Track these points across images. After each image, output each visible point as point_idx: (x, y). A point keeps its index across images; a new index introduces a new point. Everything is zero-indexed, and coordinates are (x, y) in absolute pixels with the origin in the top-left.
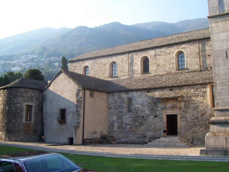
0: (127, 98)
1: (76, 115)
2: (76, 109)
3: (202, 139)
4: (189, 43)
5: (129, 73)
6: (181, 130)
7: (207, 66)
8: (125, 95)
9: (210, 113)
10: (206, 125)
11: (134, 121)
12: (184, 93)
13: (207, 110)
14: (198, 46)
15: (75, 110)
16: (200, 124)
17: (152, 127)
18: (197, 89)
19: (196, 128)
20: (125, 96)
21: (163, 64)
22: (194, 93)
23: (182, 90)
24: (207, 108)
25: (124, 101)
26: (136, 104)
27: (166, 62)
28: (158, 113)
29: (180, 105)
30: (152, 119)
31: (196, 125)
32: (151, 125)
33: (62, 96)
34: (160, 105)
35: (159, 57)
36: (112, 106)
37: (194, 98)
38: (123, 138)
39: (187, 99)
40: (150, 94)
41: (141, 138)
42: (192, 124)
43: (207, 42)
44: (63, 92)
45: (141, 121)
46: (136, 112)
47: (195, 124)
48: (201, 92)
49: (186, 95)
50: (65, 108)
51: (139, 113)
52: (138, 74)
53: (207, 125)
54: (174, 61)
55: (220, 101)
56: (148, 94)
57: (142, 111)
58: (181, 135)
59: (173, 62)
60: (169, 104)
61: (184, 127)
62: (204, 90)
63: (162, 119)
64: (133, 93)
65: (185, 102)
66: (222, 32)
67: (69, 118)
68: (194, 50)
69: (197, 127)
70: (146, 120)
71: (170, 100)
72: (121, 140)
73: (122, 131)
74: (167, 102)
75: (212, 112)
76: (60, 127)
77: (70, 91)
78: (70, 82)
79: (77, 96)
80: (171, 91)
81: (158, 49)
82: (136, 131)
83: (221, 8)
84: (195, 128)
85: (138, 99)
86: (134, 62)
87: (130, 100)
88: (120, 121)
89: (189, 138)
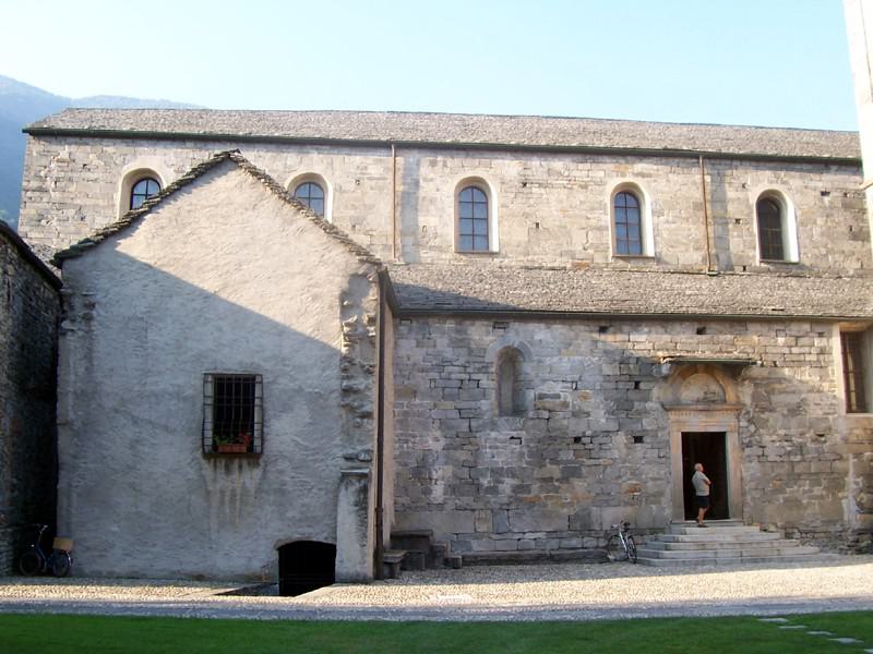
0: (499, 348)
1: (336, 412)
2: (343, 378)
5: (398, 241)
7: (729, 258)
8: (488, 333)
9: (845, 432)
11: (539, 458)
12: (750, 346)
13: (834, 419)
15: (335, 384)
16: (813, 470)
18: (797, 337)
19: (800, 486)
20: (491, 338)
21: (557, 223)
22: (786, 350)
23: (746, 334)
24: (834, 413)
25: (486, 360)
26: (544, 381)
27: (570, 217)
28: (647, 423)
29: (738, 397)
30: (625, 451)
31: (799, 475)
32: (620, 477)
33: (232, 299)
34: (658, 392)
35: (543, 191)
36: (421, 381)
37: (787, 372)
38: (477, 535)
39: (765, 372)
40: (612, 339)
41: (572, 536)
42: (783, 470)
43: (729, 172)
44: (237, 276)
45: (571, 456)
46: (546, 415)
47: (797, 470)
48: (813, 350)
49: (761, 355)
50: (251, 371)
51: (564, 421)
52: (440, 249)
53: (836, 476)
54: (603, 217)
56: (603, 337)
57: (575, 415)
59: (603, 223)
60: (692, 391)
61: (753, 485)
63: (665, 448)
64: (532, 326)
65: (756, 385)
67: (282, 429)
69: (801, 482)
70: (594, 454)
71: (696, 372)
72: (470, 549)
73: (474, 505)
74: (684, 379)
75: (851, 429)
76: (215, 480)
77: (293, 275)
78: (294, 227)
79: (345, 311)
80: (699, 336)
81: (535, 158)
82: (549, 502)
84: (795, 487)
85: (556, 359)
86: (421, 193)
87: (511, 359)
88: (462, 455)
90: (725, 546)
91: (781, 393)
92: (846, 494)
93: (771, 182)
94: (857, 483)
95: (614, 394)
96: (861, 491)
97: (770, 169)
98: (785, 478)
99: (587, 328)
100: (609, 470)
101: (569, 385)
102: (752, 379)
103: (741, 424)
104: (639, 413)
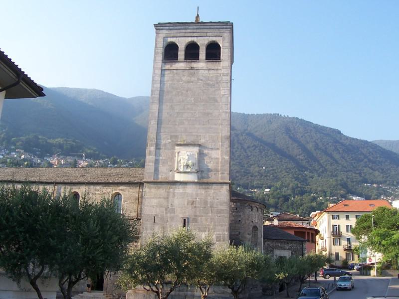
4: (129, 185)
6: (107, 284)
55: (222, 178)
66: (153, 198)
83: (156, 175)
89: (115, 295)
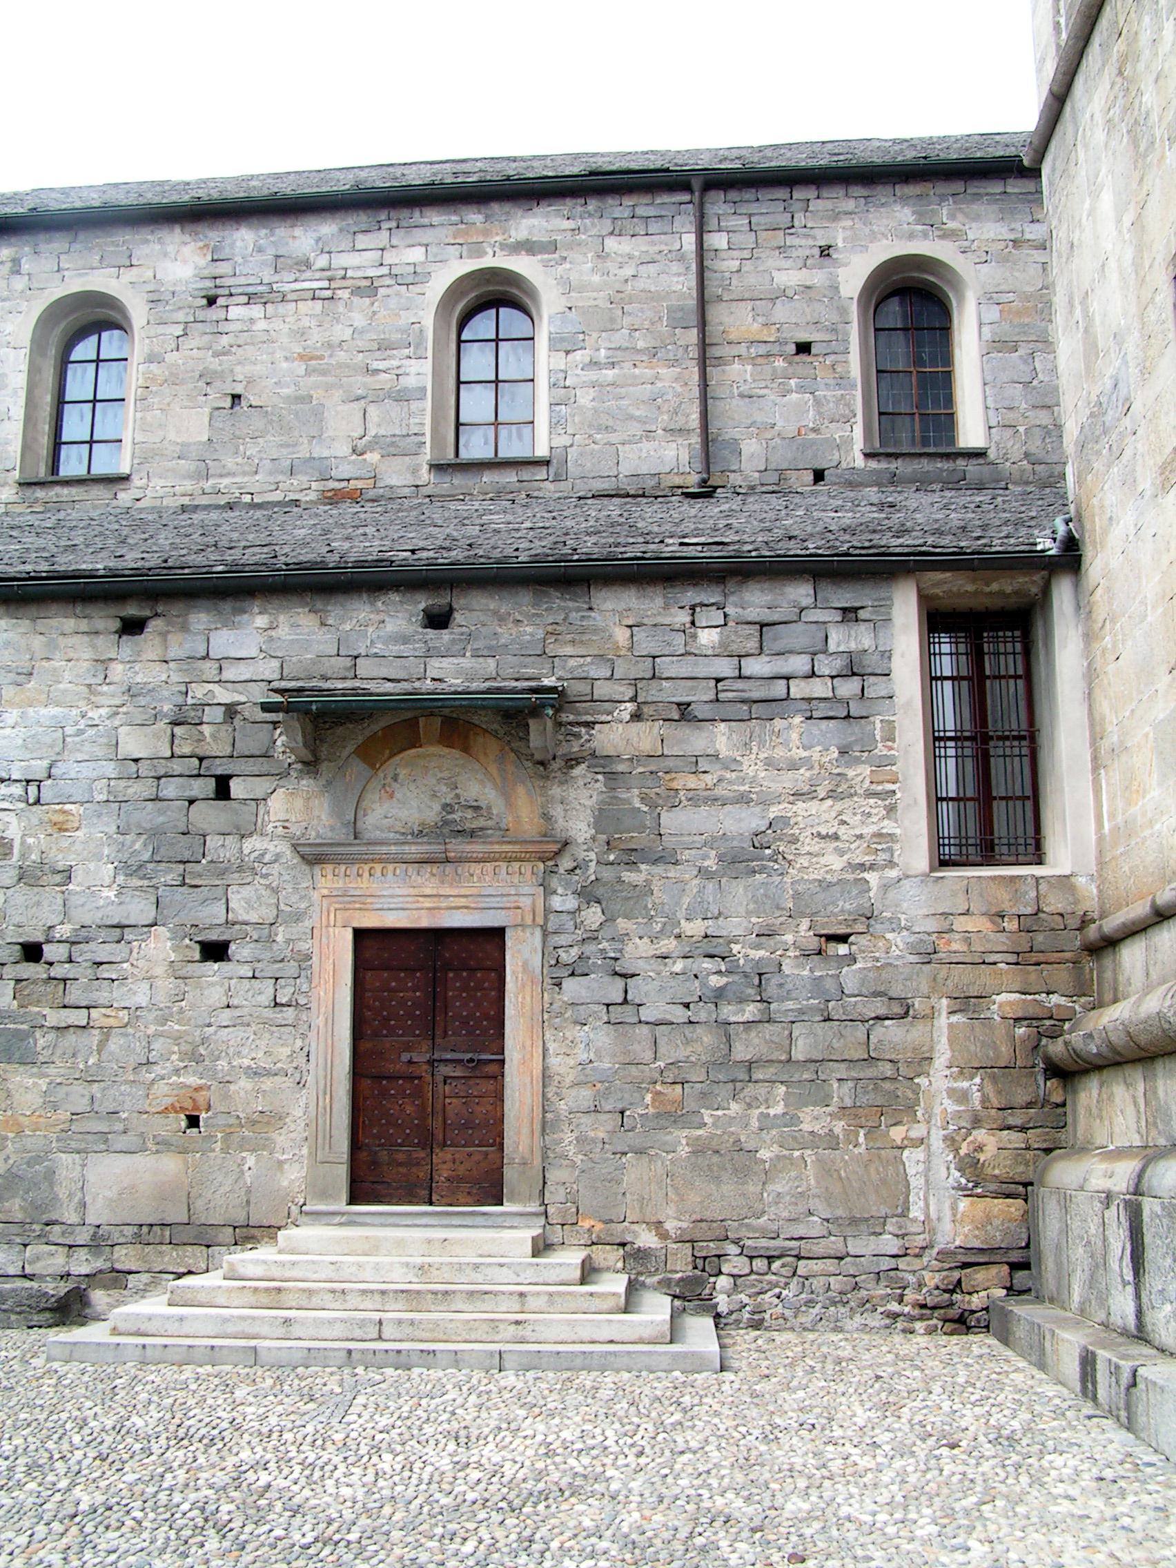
3: (819, 1248)
10: (870, 1072)
13: (885, 887)
14: (689, 241)
16: (799, 1054)
17: (161, 1088)
22: (725, 667)
24: (891, 864)
27: (324, 373)
29: (546, 817)
30: (166, 985)
31: (750, 1065)
35: (256, 311)
48: (825, 666)
53: (888, 1069)
54: (413, 366)
58: (555, 1195)
59: (410, 382)
61: (585, 1096)
62: (858, 639)
65: (611, 776)
68: (641, 284)
70: (75, 994)
71: (414, 743)
84: (735, 1107)
89: (646, 1239)
90: (353, 1301)
91: (696, 800)
92: (918, 1131)
93: (911, 236)
94: (962, 1097)
95: (149, 815)
96: (976, 1122)
97: (904, 200)
98: (697, 1075)
99: (84, 625)
100: (114, 1045)
101: (17, 790)
102: (602, 763)
103: (556, 902)
104: (221, 870)
